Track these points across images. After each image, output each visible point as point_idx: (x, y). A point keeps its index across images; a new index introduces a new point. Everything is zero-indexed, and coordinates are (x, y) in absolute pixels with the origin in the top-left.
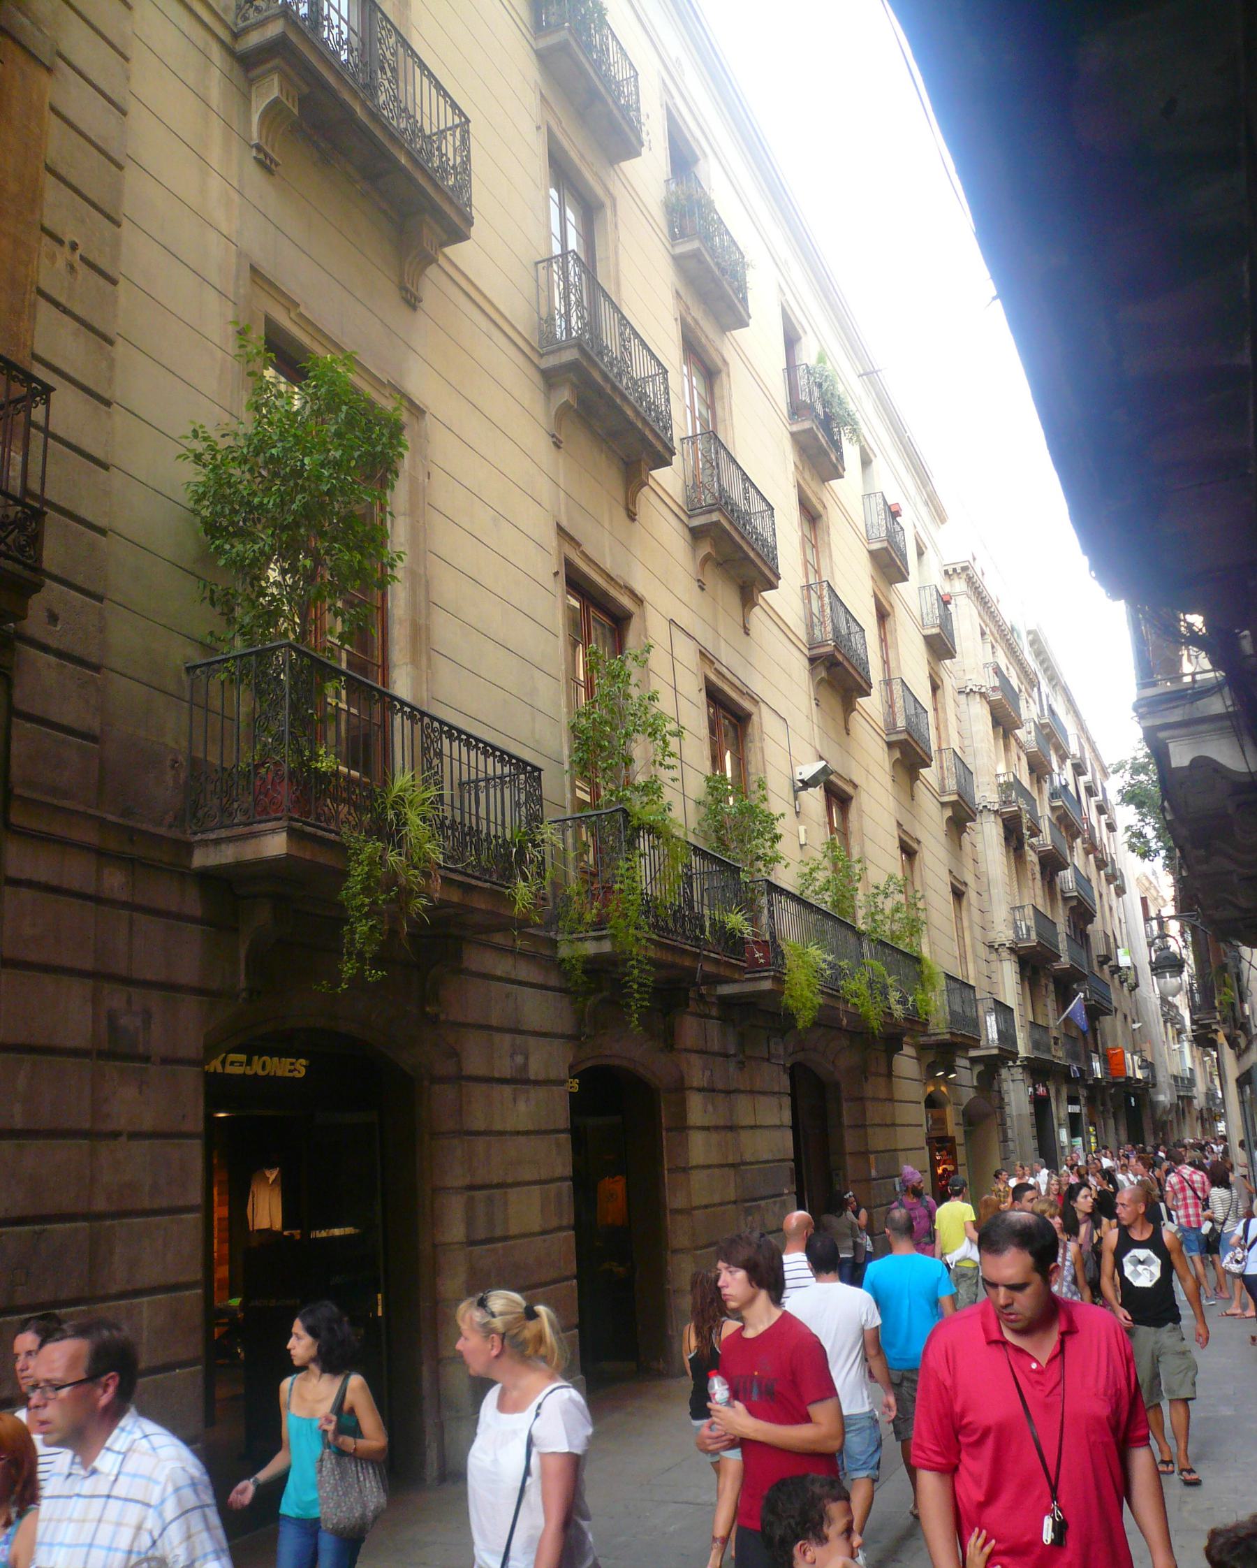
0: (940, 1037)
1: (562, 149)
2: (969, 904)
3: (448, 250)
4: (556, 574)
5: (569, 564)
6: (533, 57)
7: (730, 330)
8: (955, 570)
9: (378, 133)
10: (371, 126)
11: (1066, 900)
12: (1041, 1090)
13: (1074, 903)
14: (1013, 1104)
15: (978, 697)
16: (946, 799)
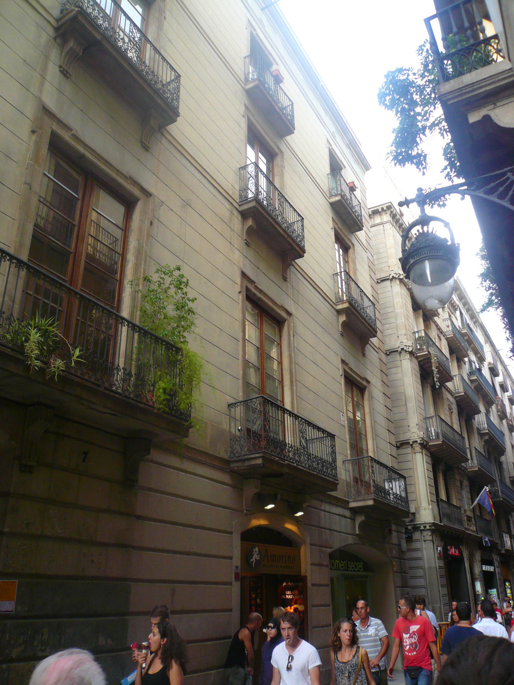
0: (253, 462)
1: (253, 124)
2: (371, 397)
3: (296, 261)
4: (240, 292)
5: (247, 289)
6: (244, 93)
7: (355, 232)
8: (382, 209)
9: (148, 90)
10: (130, 70)
11: (481, 435)
12: (453, 551)
13: (487, 437)
14: (425, 558)
15: (398, 282)
16: (340, 307)
